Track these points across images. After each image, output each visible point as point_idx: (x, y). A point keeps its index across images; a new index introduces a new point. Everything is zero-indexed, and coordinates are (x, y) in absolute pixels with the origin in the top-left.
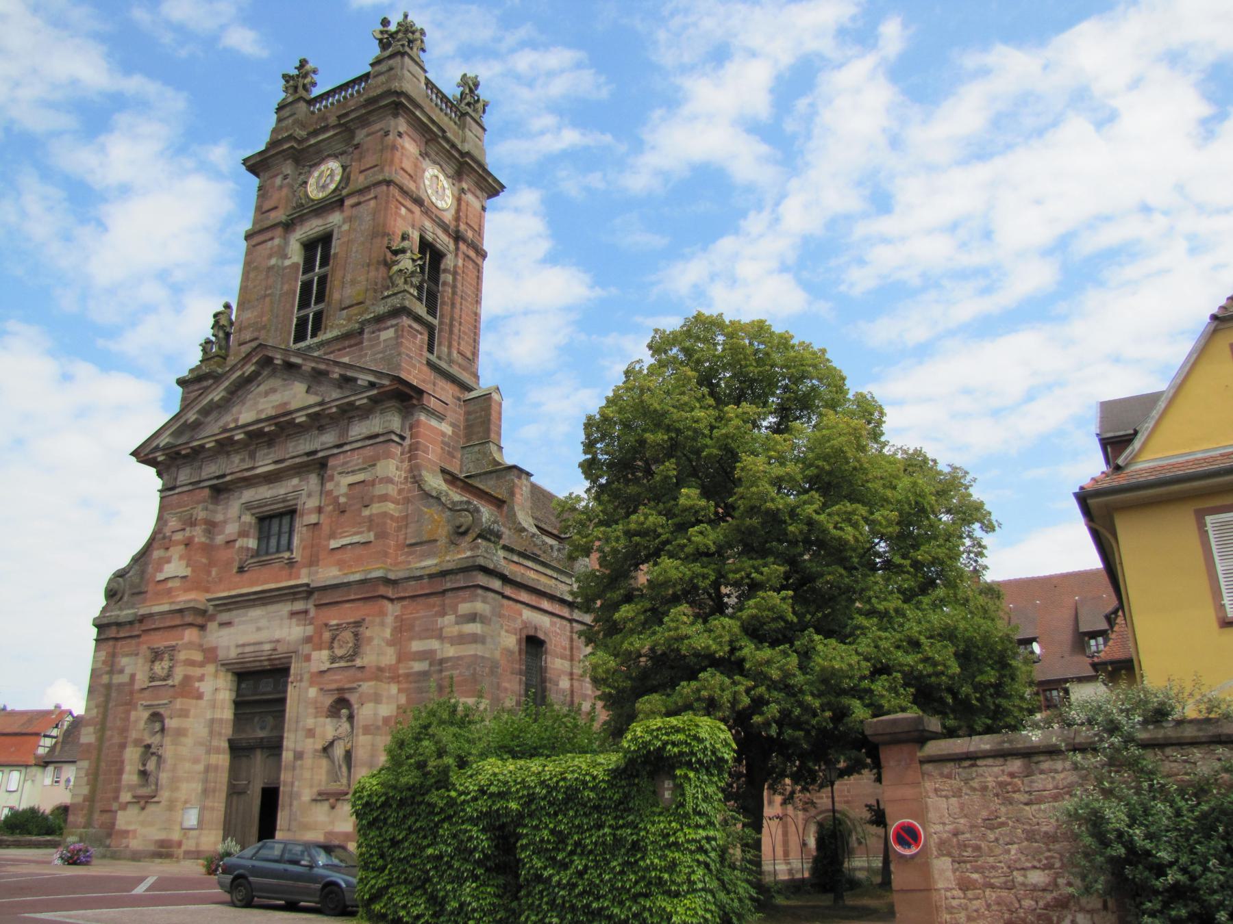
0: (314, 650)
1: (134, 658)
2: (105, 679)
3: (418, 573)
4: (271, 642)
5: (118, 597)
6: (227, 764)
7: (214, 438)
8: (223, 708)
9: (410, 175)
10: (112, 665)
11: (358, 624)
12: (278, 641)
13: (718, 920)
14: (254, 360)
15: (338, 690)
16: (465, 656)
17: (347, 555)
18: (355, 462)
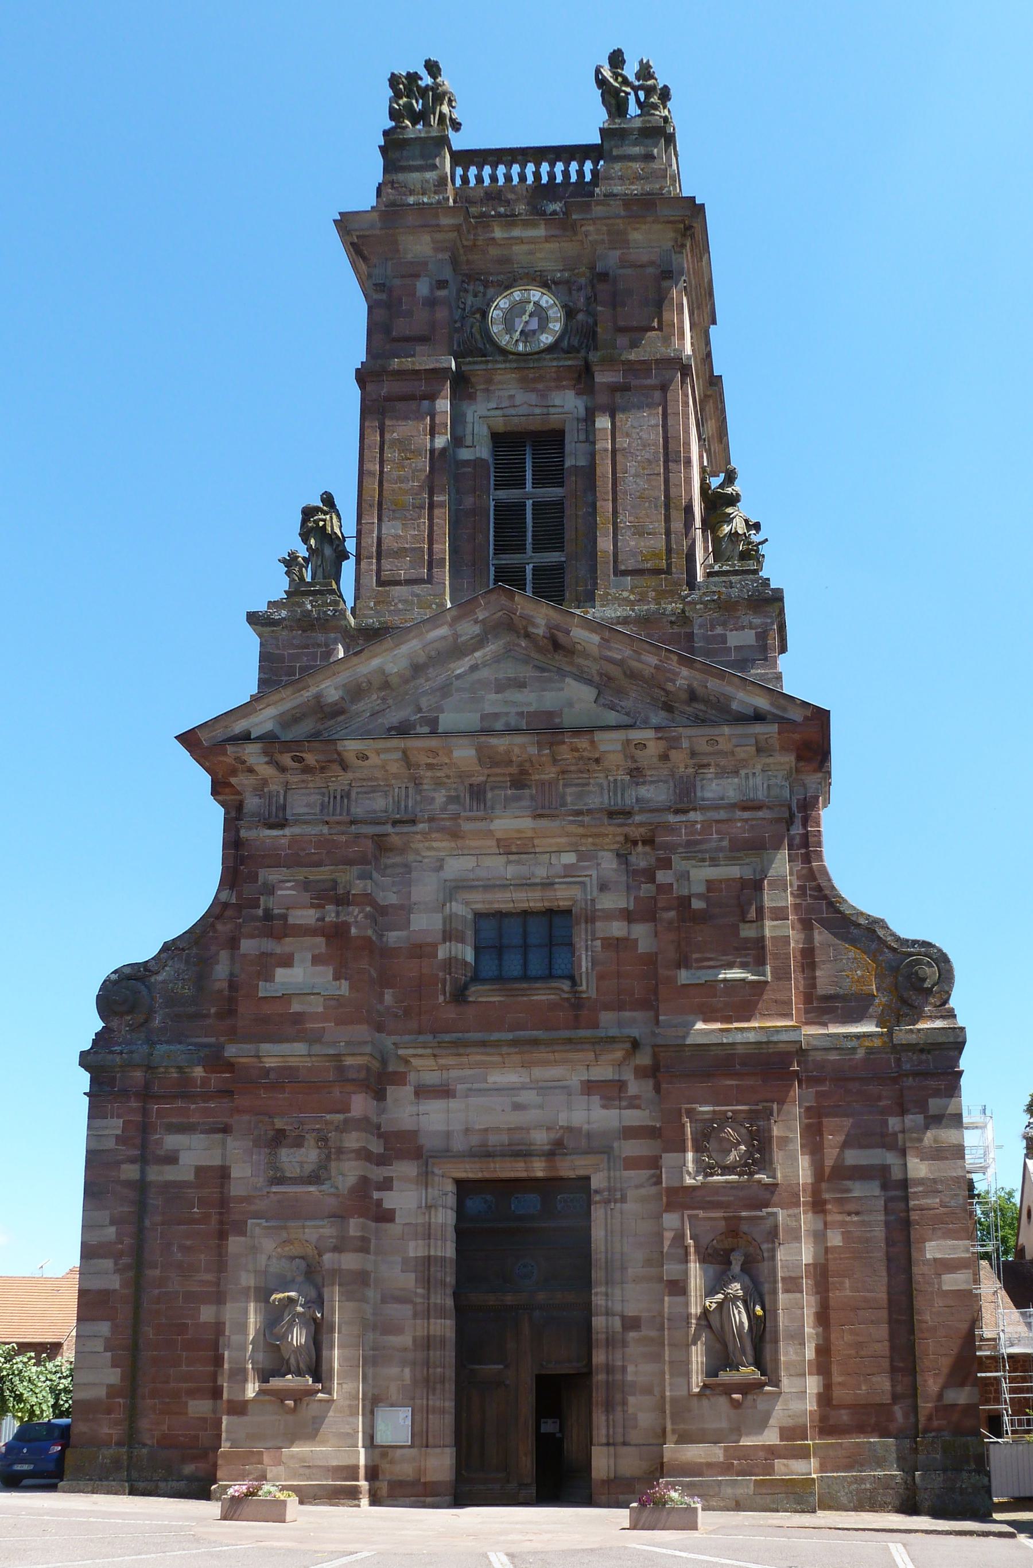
0: (666, 1150)
1: (220, 1136)
2: (130, 1172)
4: (548, 1129)
6: (450, 1334)
8: (444, 1240)
9: (510, 407)
10: (144, 1146)
12: (569, 1129)
14: (481, 616)
18: (714, 844)
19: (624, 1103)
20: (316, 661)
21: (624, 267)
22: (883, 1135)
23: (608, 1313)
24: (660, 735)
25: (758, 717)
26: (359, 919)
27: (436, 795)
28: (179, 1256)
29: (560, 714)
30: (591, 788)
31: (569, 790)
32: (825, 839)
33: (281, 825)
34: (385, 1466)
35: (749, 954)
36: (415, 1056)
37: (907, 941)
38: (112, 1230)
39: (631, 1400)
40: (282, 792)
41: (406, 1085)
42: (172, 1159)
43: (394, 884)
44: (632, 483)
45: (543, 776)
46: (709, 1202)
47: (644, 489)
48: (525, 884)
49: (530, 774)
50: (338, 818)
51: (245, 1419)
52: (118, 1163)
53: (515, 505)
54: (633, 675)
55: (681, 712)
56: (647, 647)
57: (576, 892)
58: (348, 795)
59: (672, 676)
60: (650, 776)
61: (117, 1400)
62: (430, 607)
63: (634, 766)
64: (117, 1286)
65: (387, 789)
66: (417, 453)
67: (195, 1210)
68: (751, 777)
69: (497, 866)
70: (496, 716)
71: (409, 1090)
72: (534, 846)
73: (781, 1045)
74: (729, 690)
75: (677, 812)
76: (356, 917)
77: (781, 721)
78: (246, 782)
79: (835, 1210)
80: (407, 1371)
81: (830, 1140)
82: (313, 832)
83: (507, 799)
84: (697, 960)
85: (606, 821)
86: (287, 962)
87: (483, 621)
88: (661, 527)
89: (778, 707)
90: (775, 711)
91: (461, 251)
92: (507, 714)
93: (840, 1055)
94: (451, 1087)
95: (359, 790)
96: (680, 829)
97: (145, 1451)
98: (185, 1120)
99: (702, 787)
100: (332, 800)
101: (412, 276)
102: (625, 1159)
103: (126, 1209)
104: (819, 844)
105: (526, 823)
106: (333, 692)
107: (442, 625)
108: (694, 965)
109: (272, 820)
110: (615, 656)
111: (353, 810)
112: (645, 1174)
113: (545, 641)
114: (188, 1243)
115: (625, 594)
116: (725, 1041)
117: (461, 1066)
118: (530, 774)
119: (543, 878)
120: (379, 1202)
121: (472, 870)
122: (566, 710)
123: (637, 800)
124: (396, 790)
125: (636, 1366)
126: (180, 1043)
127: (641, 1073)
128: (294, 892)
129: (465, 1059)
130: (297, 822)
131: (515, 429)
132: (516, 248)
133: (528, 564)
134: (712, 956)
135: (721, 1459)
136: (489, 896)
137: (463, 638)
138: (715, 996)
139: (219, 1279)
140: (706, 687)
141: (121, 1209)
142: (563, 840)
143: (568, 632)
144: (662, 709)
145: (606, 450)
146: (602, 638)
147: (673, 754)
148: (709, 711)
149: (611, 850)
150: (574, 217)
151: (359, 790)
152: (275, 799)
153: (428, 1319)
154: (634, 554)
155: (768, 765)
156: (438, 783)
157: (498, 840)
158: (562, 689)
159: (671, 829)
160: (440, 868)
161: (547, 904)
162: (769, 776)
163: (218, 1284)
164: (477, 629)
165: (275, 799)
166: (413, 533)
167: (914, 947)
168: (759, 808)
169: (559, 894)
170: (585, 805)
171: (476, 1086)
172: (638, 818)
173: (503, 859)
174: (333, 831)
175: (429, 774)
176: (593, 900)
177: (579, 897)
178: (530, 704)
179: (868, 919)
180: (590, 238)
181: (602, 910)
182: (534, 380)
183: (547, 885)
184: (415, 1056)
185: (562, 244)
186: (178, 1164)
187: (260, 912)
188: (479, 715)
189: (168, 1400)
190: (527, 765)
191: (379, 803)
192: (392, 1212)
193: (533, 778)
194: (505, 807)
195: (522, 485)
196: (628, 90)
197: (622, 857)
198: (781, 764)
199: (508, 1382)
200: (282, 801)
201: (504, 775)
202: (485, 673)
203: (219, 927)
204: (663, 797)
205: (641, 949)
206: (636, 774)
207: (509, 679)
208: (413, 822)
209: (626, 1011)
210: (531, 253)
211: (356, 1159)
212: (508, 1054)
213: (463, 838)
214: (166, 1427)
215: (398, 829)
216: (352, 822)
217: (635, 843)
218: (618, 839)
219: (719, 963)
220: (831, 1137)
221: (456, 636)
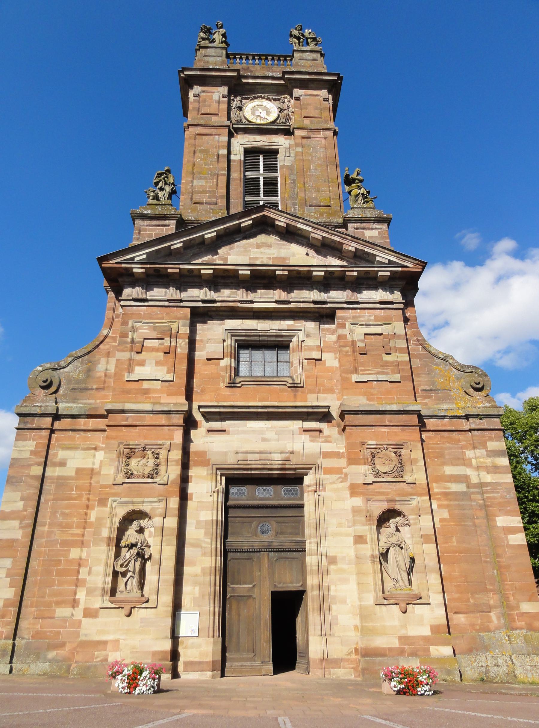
3: (442, 413)
4: (282, 452)
5: (53, 389)
7: (251, 268)
11: (399, 446)
12: (292, 452)
13: (2, 725)
15: (388, 501)
16: (503, 483)
17: (375, 387)
18: (367, 318)
19: (322, 440)
20: (163, 232)
22: (463, 459)
23: (319, 554)
28: (61, 519)
35: (389, 369)
37: (465, 365)
38: (22, 503)
39: (334, 607)
42: (63, 464)
46: (377, 492)
52: (30, 466)
53: (256, 178)
61: (10, 609)
62: (218, 214)
64: (20, 537)
67: (74, 492)
76: (180, 344)
80: (197, 588)
86: (142, 364)
92: (262, 258)
97: (24, 642)
98: (73, 443)
102: (324, 468)
103: (31, 492)
108: (360, 372)
114: (67, 511)
115: (313, 214)
125: (336, 586)
126: (74, 402)
134: (369, 369)
135: (398, 646)
138: (372, 387)
139: (84, 532)
141: (28, 491)
153: (211, 557)
163: (83, 535)
167: (468, 369)
178: (274, 254)
179: (443, 355)
187: (129, 340)
188: (248, 257)
189: (42, 608)
199: (255, 596)
207: (263, 243)
211: (176, 465)
214: (39, 626)
219: (372, 372)
220: (436, 460)
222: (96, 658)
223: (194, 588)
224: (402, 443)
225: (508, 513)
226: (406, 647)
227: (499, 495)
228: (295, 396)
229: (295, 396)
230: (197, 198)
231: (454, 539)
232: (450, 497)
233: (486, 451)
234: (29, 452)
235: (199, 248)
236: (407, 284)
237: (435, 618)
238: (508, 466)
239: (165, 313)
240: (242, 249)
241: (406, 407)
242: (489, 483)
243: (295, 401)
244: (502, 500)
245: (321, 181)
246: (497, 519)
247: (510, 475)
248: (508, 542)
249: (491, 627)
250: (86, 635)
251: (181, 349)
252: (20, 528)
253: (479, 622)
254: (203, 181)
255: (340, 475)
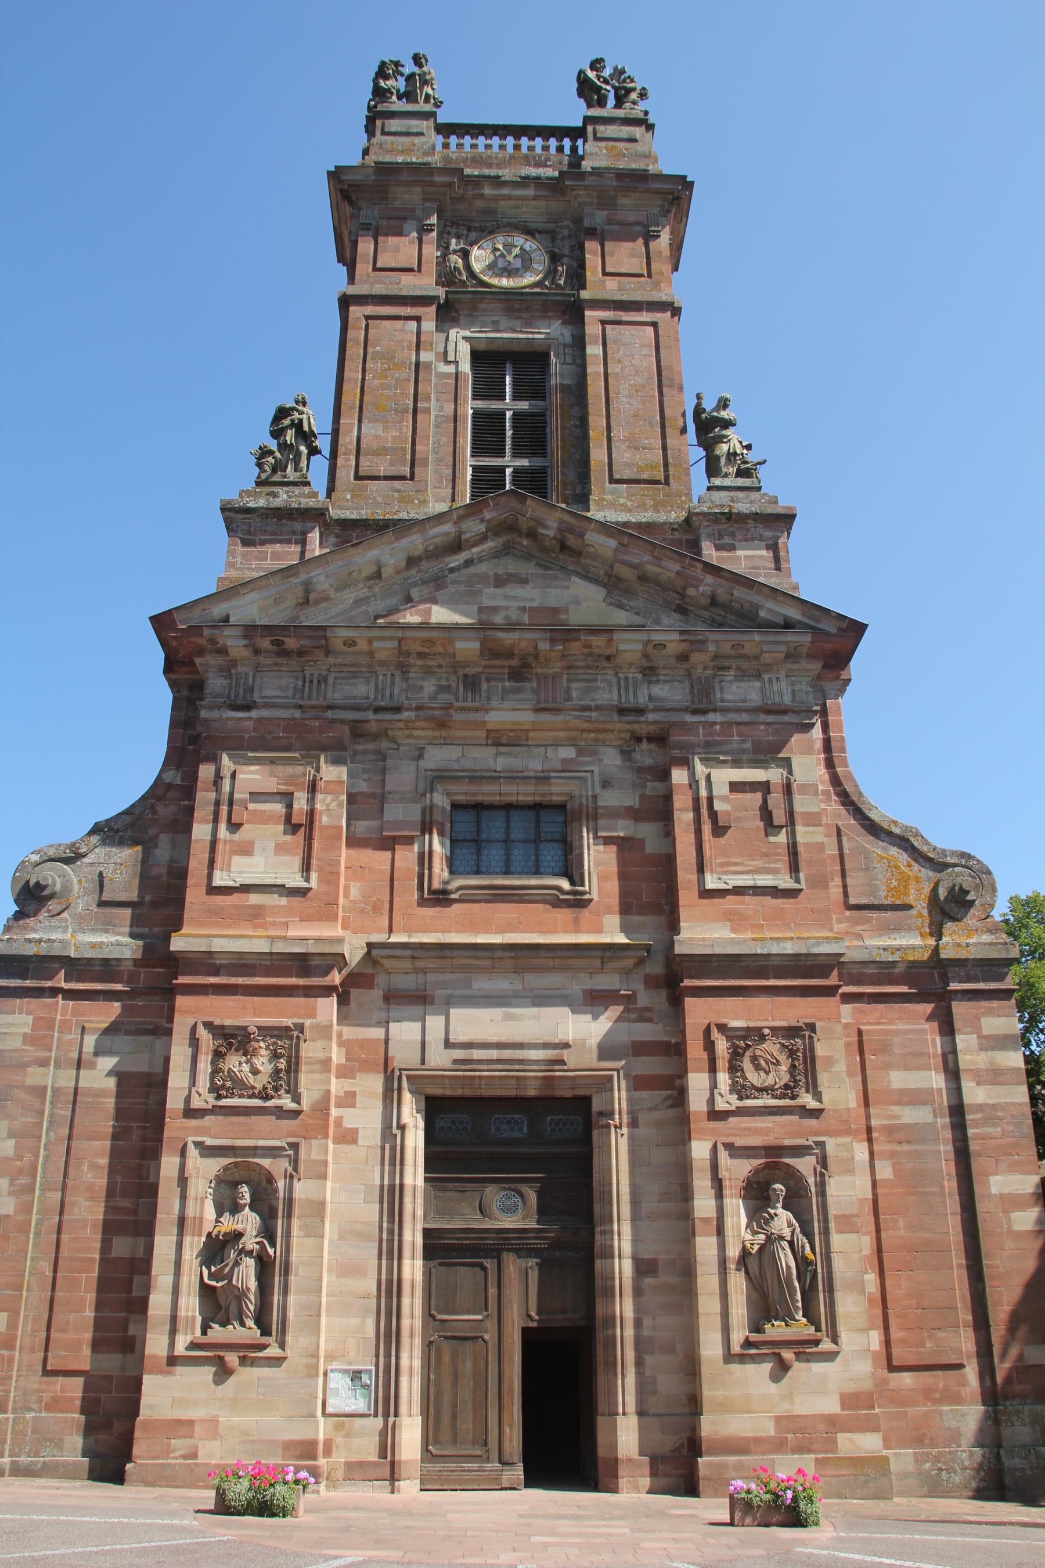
1: (147, 1038)
14: (488, 516)
18: (735, 746)
21: (610, 224)
24: (685, 637)
25: (788, 625)
26: (331, 807)
27: (425, 684)
29: (566, 611)
30: (599, 684)
31: (574, 685)
32: (848, 745)
33: (248, 708)
34: (339, 1440)
35: (780, 860)
36: (389, 957)
40: (251, 674)
41: (373, 988)
43: (364, 771)
44: (624, 403)
45: (545, 670)
46: (745, 1129)
47: (639, 409)
48: (514, 777)
49: (532, 668)
50: (314, 702)
51: (170, 1379)
54: (643, 578)
55: (696, 615)
56: (669, 554)
57: (574, 788)
58: (325, 680)
59: (695, 583)
60: (664, 675)
63: (648, 664)
65: (368, 675)
66: (400, 366)
68: (774, 682)
69: (485, 758)
70: (495, 609)
71: (377, 993)
72: (527, 739)
73: (820, 958)
74: (757, 599)
75: (695, 712)
77: (816, 632)
78: (212, 662)
79: (882, 1139)
81: (871, 1060)
82: (283, 716)
83: (504, 690)
84: (722, 865)
85: (616, 718)
86: (246, 850)
87: (489, 521)
88: (659, 443)
89: (810, 618)
90: (806, 621)
91: (448, 201)
92: (507, 608)
93: (878, 968)
94: (428, 993)
95: (338, 675)
96: (697, 729)
99: (721, 688)
100: (307, 684)
101: (397, 218)
104: (843, 750)
105: (526, 717)
106: (322, 579)
107: (447, 522)
109: (239, 702)
110: (632, 560)
111: (329, 695)
112: (659, 1095)
113: (554, 542)
115: (622, 501)
116: (759, 952)
117: (442, 970)
118: (532, 668)
119: (537, 772)
120: (339, 1121)
121: (458, 760)
122: (572, 607)
123: (650, 698)
124: (381, 677)
126: (106, 931)
127: (651, 982)
128: (259, 777)
129: (448, 962)
130: (266, 706)
131: (502, 349)
132: (502, 203)
133: (508, 467)
134: (737, 860)
135: (772, 1433)
136: (474, 788)
137: (468, 535)
139: (137, 1205)
140: (732, 594)
142: (562, 734)
143: (582, 536)
144: (675, 611)
145: (598, 374)
146: (619, 543)
147: (696, 657)
148: (729, 616)
149: (615, 746)
150: (567, 183)
151: (338, 675)
152: (242, 681)
154: (629, 465)
155: (792, 670)
156: (428, 672)
157: (489, 731)
158: (568, 587)
159: (683, 726)
160: (420, 757)
161: (538, 799)
162: (792, 682)
164: (482, 528)
165: (242, 681)
166: (394, 434)
168: (784, 712)
169: (554, 789)
170: (592, 700)
171: (458, 992)
172: (651, 717)
173: (493, 750)
174: (308, 715)
175: (419, 662)
176: (595, 797)
177: (577, 793)
178: (533, 600)
180: (579, 200)
181: (605, 808)
182: (520, 310)
183: (543, 779)
184: (389, 957)
185: (550, 203)
186: (95, 1068)
190: (530, 659)
191: (362, 690)
192: (356, 1131)
193: (534, 671)
194: (502, 699)
195: (503, 398)
196: (608, 88)
197: (626, 754)
198: (806, 670)
200: (250, 683)
201: (503, 667)
202: (482, 568)
203: (160, 809)
204: (678, 697)
205: (648, 850)
206: (650, 672)
207: (510, 575)
208: (398, 709)
209: (632, 914)
210: (516, 207)
212: (501, 958)
213: (449, 727)
215: (379, 716)
216: (329, 707)
217: (639, 740)
218: (623, 735)
220: (873, 1057)
221: (460, 533)
222: (174, 1451)
223: (363, 1322)
224: (801, 1024)
225: (1015, 1168)
226: (790, 1436)
227: (999, 1129)
228: (576, 921)
229: (576, 921)
230: (367, 465)
231: (901, 1224)
232: (898, 1136)
233: (979, 1037)
234: (21, 1038)
235: (369, 587)
236: (825, 666)
237: (851, 1380)
238: (1019, 1069)
239: (295, 736)
240: (463, 588)
241: (813, 946)
242: (981, 1105)
243: (577, 931)
244: (1005, 1141)
245: (641, 422)
246: (992, 1179)
247: (1024, 1089)
248: (1010, 1227)
249: (963, 1393)
250: (152, 1407)
251: (329, 816)
252: (10, 1193)
253: (941, 1385)
254: (380, 426)
255: (669, 1092)
